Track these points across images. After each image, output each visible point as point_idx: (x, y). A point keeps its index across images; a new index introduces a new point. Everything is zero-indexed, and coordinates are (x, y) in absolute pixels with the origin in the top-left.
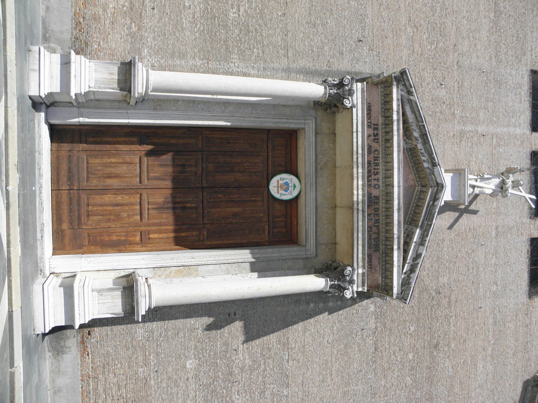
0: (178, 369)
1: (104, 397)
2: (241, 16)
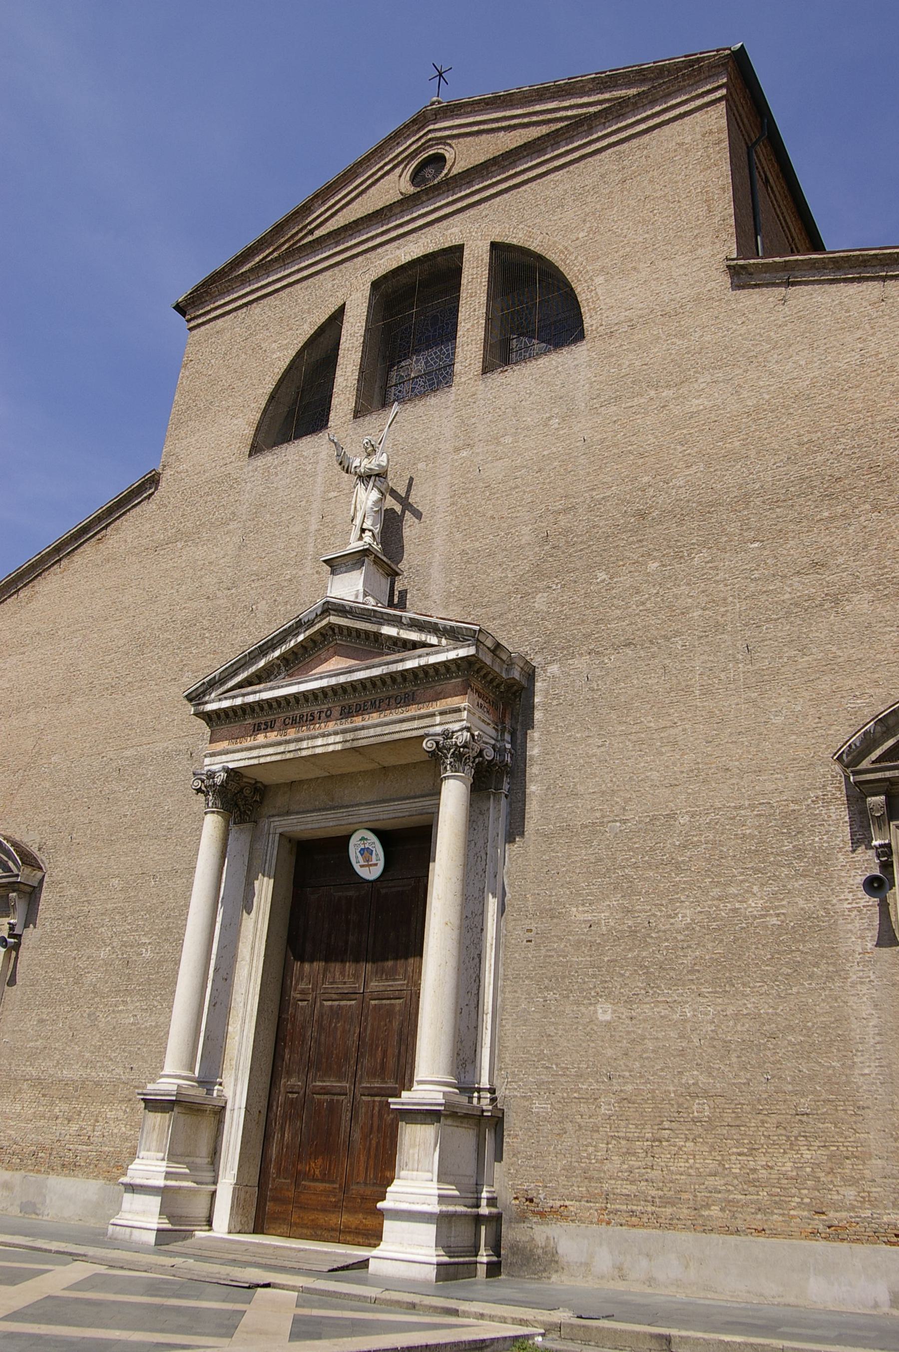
0: (611, 1036)
1: (645, 1183)
2: (151, 941)
